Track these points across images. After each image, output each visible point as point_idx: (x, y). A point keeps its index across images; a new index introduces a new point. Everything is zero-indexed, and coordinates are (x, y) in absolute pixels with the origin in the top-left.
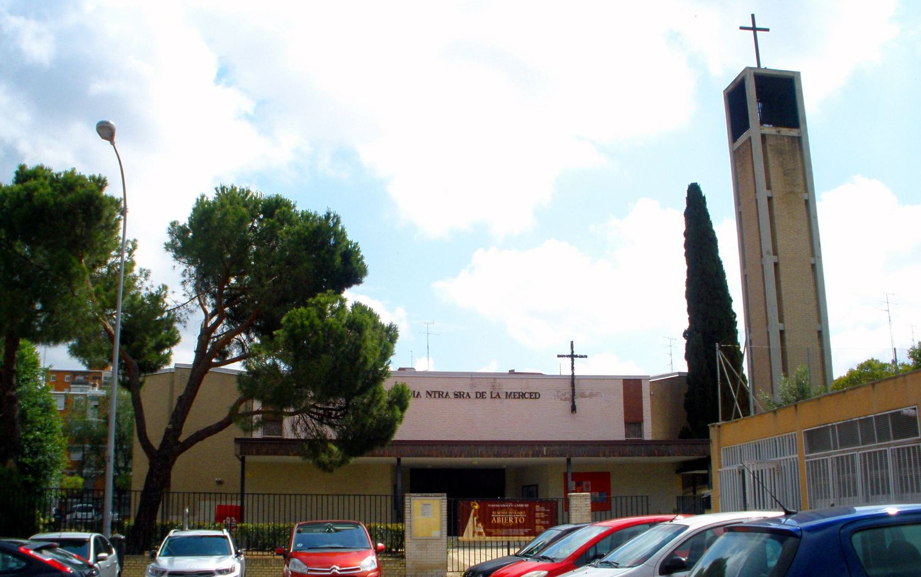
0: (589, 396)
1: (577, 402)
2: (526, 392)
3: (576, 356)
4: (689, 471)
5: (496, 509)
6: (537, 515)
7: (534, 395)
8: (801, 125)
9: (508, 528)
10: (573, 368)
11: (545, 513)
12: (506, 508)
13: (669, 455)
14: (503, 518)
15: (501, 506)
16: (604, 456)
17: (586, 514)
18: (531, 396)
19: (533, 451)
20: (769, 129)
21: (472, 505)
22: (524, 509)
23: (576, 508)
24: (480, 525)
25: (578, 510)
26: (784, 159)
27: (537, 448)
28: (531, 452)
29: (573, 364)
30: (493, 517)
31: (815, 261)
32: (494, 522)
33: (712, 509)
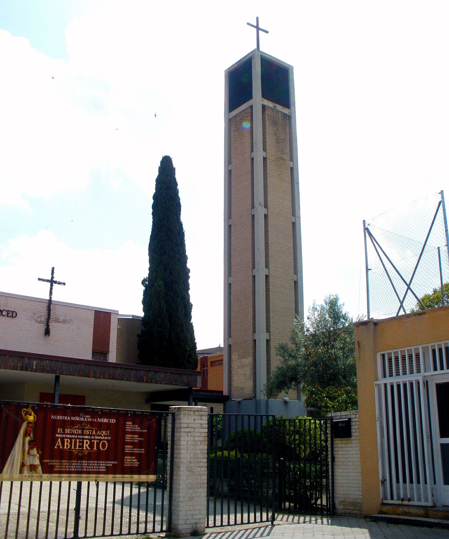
0: (62, 322)
1: (52, 325)
2: (4, 310)
3: (56, 282)
4: (154, 402)
5: (64, 424)
6: (128, 437)
7: (11, 313)
8: (292, 107)
9: (81, 458)
10: (51, 293)
11: (140, 435)
12: (81, 422)
13: (156, 382)
14: (73, 440)
15: (73, 418)
16: (94, 377)
17: (201, 439)
18: (8, 314)
19: (23, 364)
20: (266, 103)
21: (23, 414)
22: (107, 426)
23: (188, 430)
24: (34, 451)
25: (190, 432)
26: (277, 129)
27: (26, 361)
28: (20, 365)
29: (51, 289)
30: (58, 438)
31: (295, 220)
32: (59, 446)
33: (353, 438)
